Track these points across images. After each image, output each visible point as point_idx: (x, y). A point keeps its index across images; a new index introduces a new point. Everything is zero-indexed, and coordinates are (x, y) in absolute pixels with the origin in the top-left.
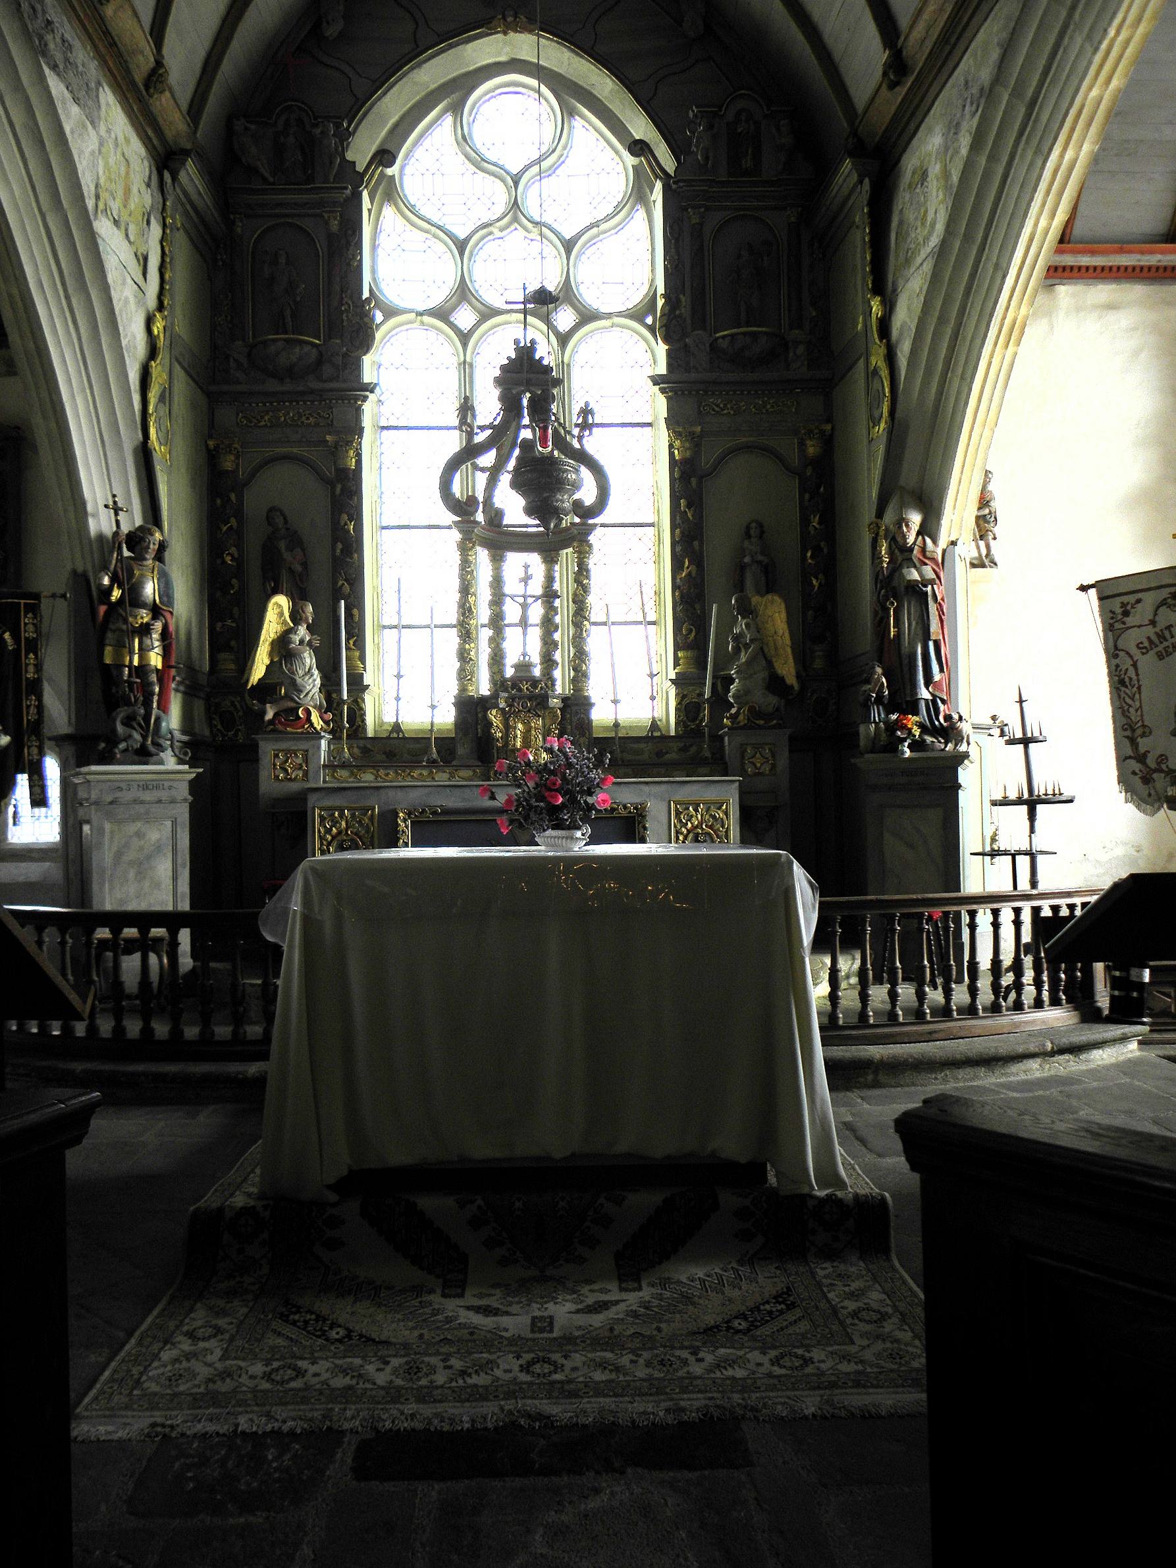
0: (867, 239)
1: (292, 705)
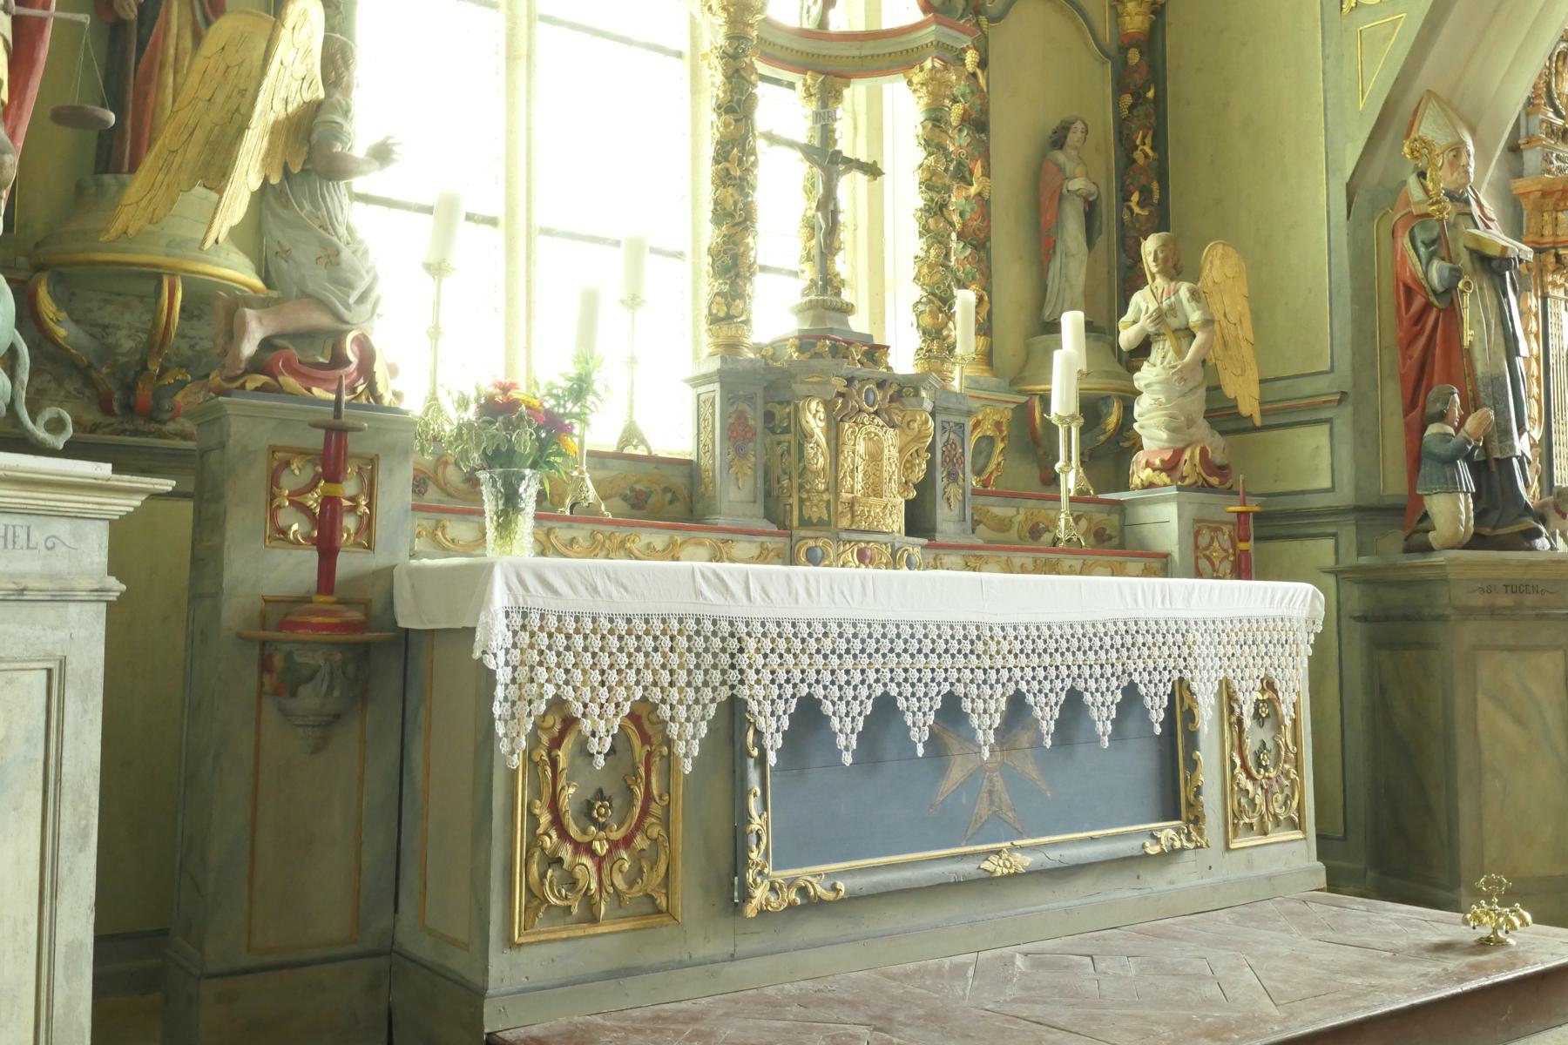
1: (321, 320)
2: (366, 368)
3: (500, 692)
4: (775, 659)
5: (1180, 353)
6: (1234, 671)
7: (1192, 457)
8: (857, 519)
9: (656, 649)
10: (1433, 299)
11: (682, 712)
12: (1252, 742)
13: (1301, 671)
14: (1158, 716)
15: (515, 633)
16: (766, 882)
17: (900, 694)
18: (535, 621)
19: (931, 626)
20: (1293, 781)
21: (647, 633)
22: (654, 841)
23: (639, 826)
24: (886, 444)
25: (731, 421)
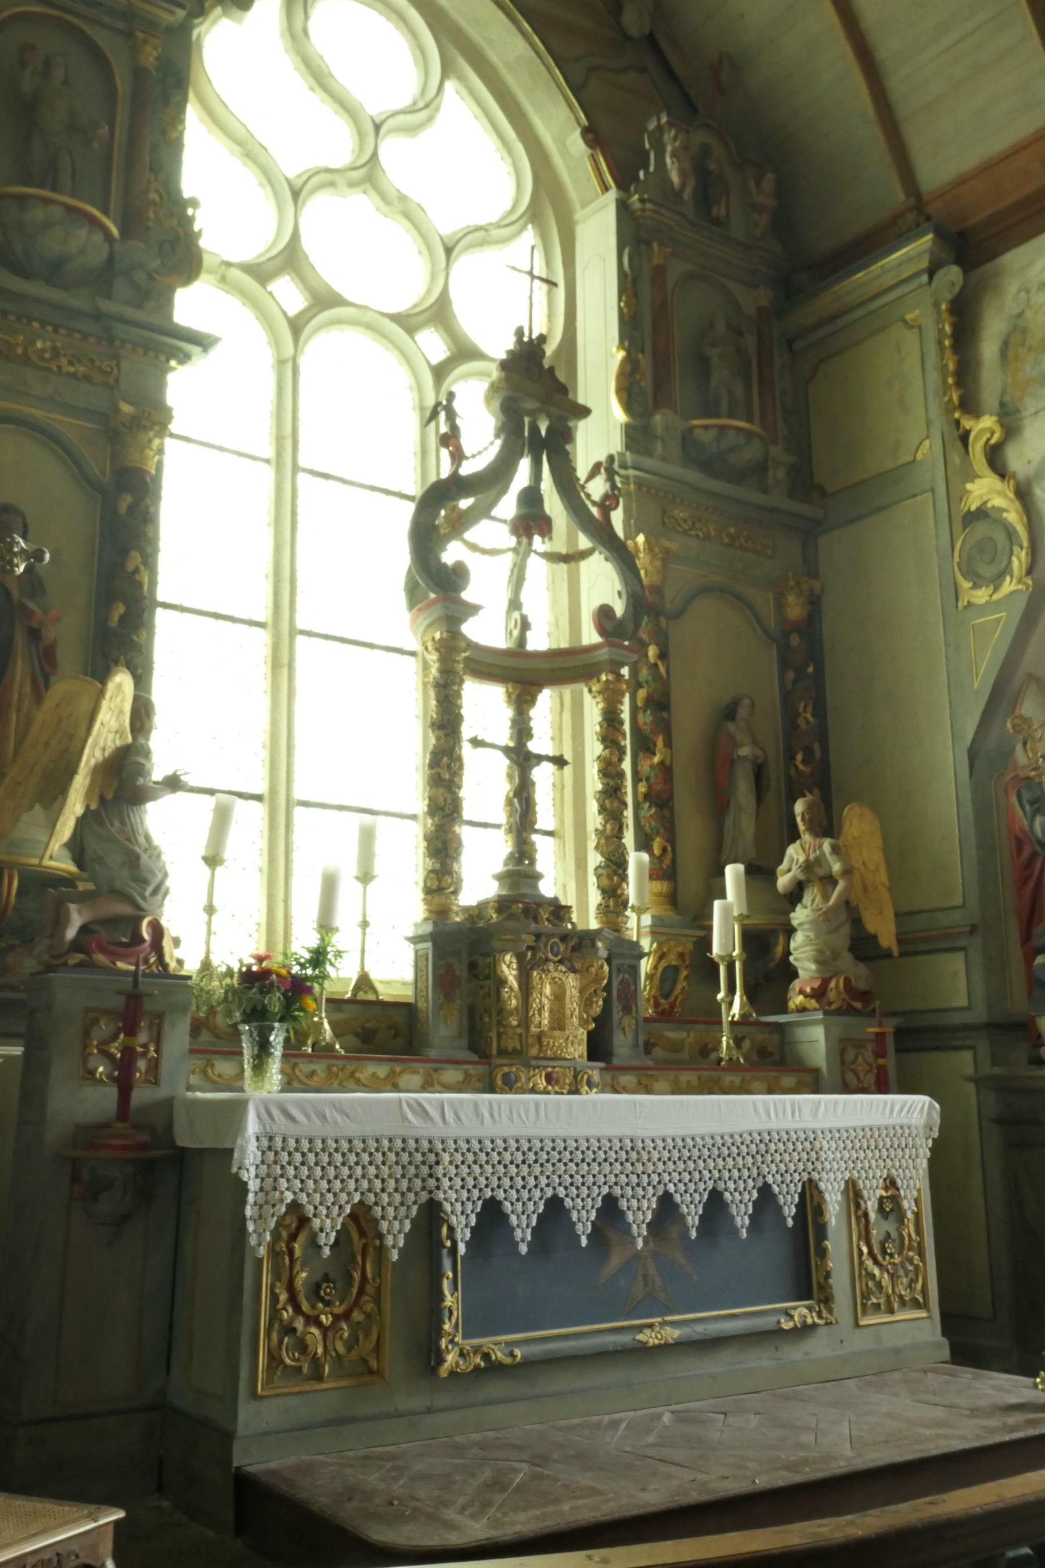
0: (947, 343)
1: (123, 909)
2: (157, 945)
3: (251, 1198)
4: (465, 1170)
5: (826, 897)
6: (858, 1172)
7: (837, 985)
8: (544, 1049)
9: (370, 1163)
10: (1038, 848)
11: (391, 1211)
12: (878, 1233)
13: (921, 1171)
14: (790, 1211)
15: (263, 1153)
16: (457, 1349)
17: (567, 1196)
18: (278, 1143)
19: (592, 1140)
20: (917, 1267)
21: (364, 1150)
22: (368, 1315)
23: (356, 1303)
24: (568, 987)
25: (441, 972)
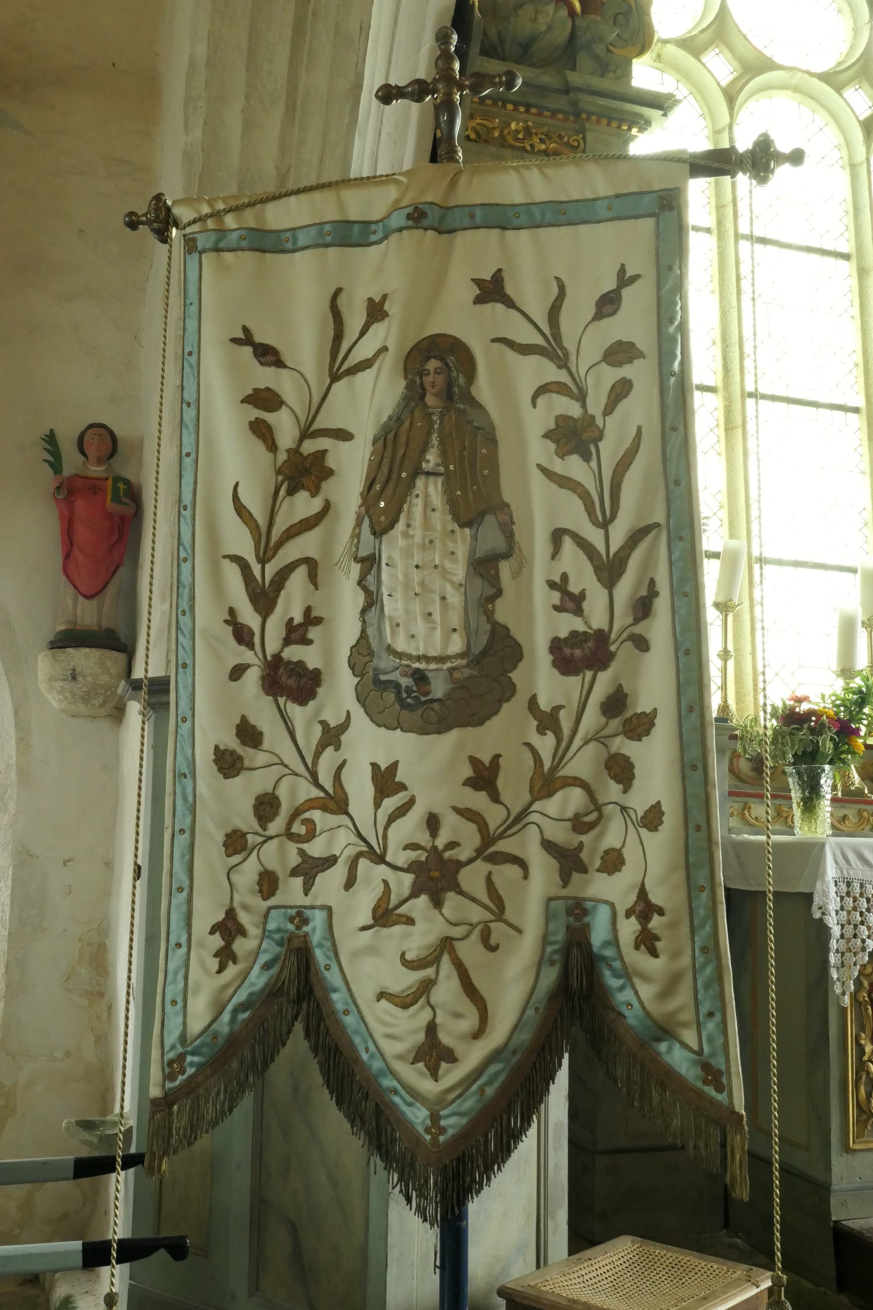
3: (833, 944)
15: (842, 898)
